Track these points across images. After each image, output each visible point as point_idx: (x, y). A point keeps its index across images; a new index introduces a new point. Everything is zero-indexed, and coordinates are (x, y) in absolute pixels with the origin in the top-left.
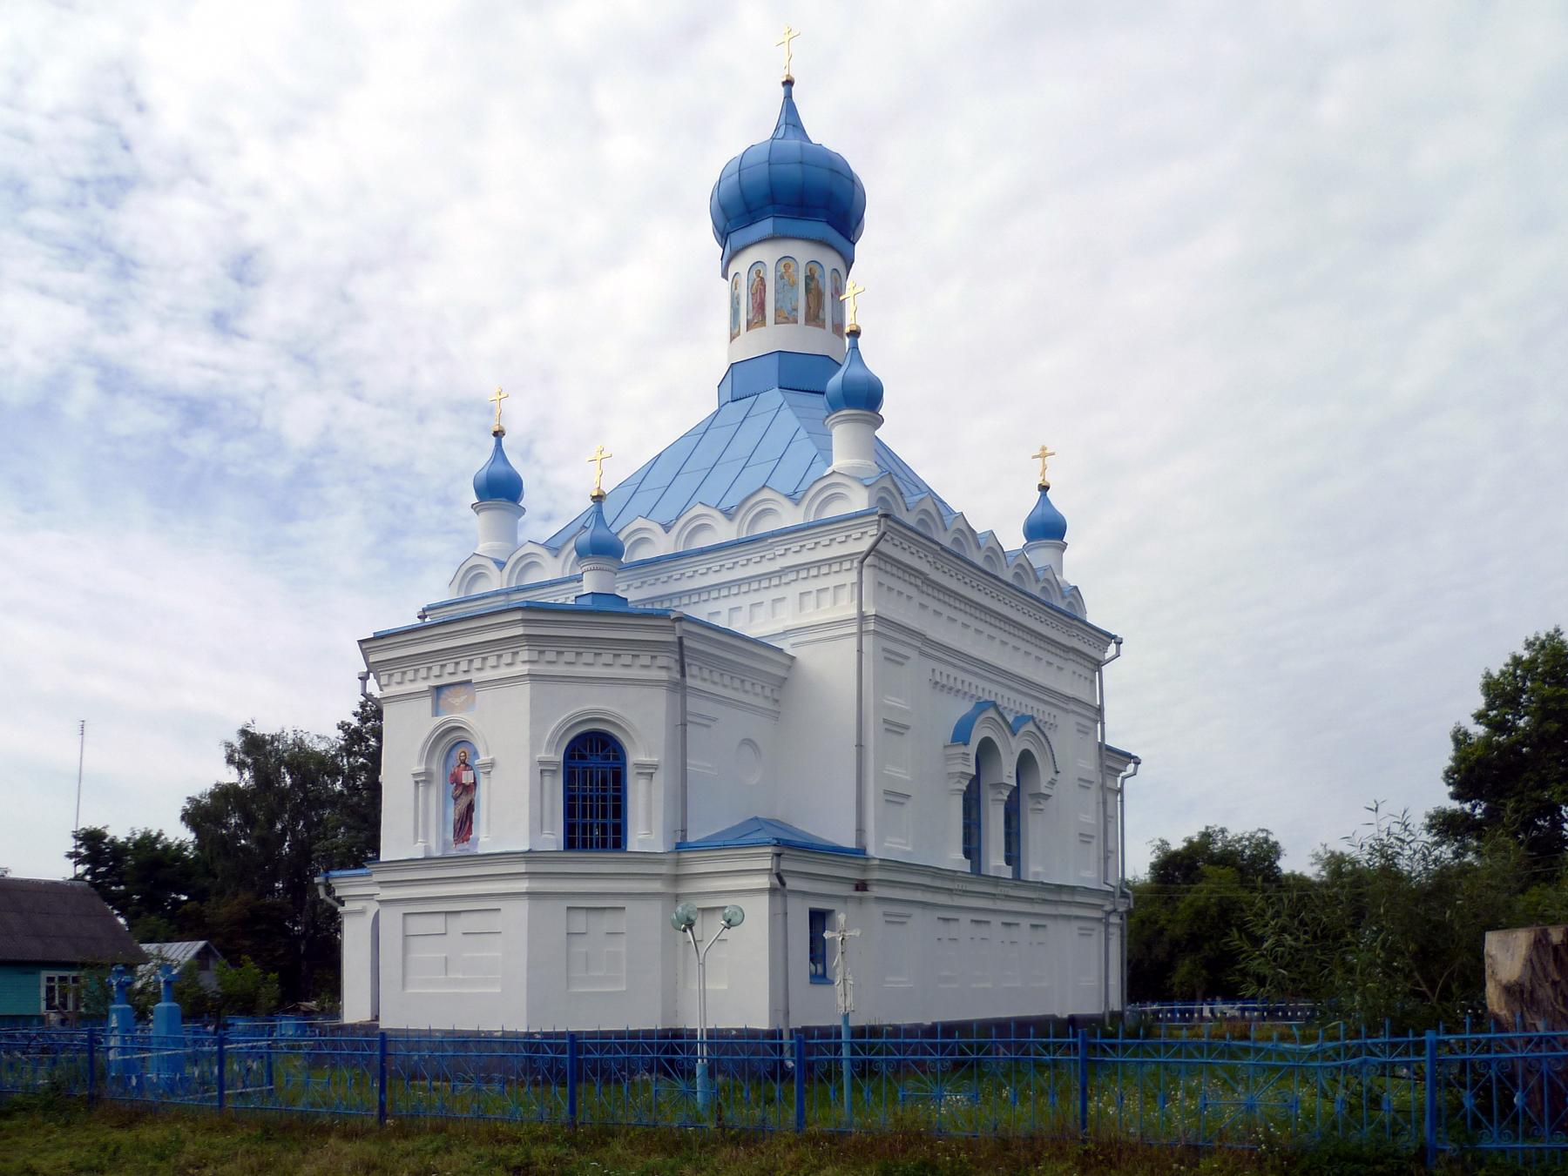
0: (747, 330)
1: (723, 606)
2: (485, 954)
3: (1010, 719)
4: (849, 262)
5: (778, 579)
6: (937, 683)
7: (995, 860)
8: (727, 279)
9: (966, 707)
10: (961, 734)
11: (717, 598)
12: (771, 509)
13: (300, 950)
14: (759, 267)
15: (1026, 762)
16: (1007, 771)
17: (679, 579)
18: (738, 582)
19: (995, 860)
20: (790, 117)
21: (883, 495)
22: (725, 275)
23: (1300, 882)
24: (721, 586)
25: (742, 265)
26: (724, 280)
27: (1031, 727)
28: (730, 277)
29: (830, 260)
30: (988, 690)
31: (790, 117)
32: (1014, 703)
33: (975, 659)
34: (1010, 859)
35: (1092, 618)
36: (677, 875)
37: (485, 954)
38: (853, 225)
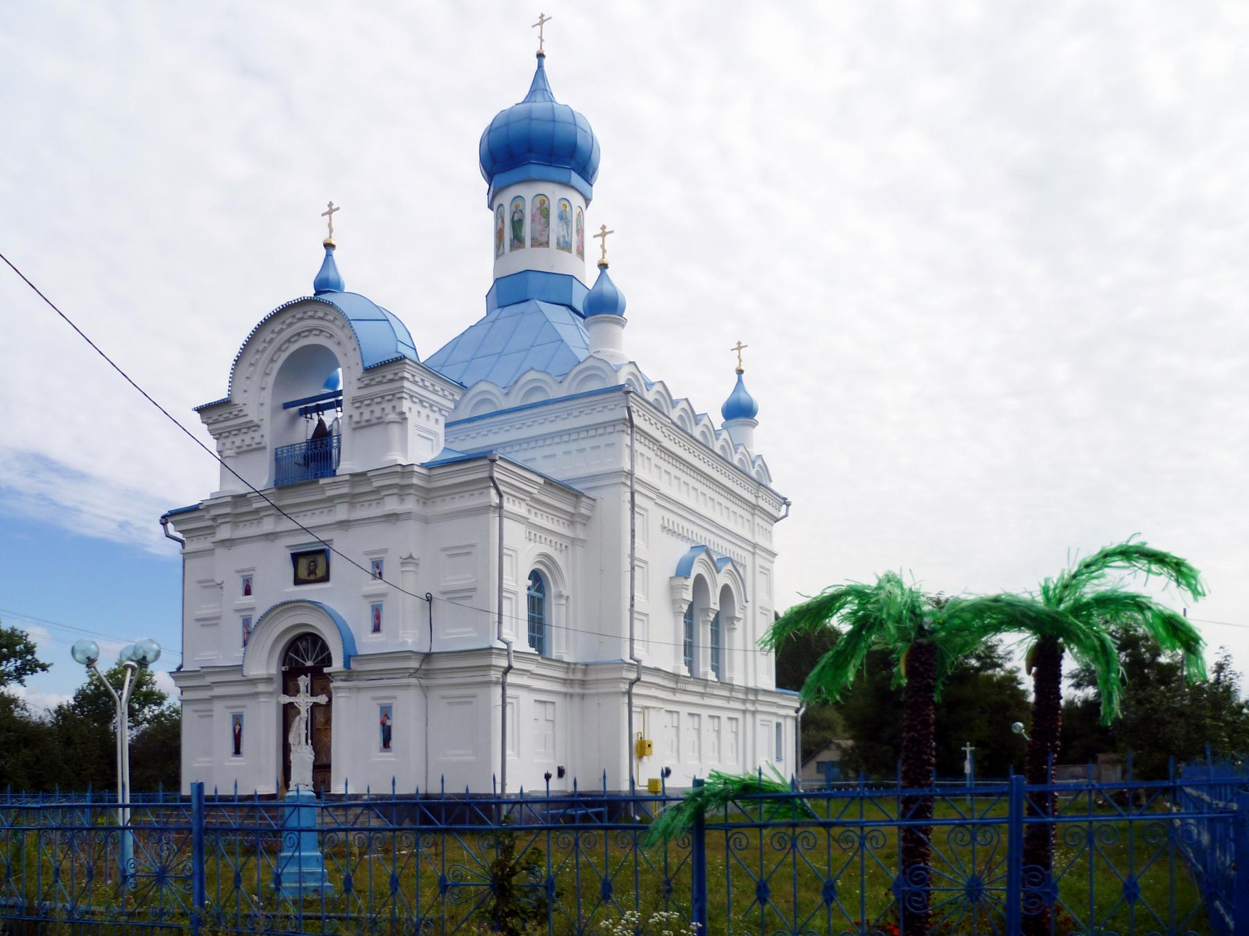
0: (200, 410)
1: (538, 453)
2: (907, 823)
3: (715, 558)
4: (587, 201)
5: (577, 435)
6: (665, 528)
7: (705, 668)
8: (492, 209)
9: (683, 549)
10: (683, 570)
11: (577, 440)
12: (542, 388)
13: (1226, 924)
14: (518, 201)
15: (726, 592)
16: (714, 602)
17: (464, 440)
18: (535, 439)
19: (705, 668)
20: (539, 83)
21: (630, 377)
22: (490, 207)
23: (299, 676)
24: (513, 443)
25: (506, 198)
26: (489, 210)
27: (729, 566)
28: (495, 207)
29: (576, 200)
30: (703, 536)
31: (539, 83)
32: (721, 546)
33: (776, 494)
34: (716, 668)
35: (772, 486)
36: (583, 681)
37: (907, 823)
38: (591, 173)
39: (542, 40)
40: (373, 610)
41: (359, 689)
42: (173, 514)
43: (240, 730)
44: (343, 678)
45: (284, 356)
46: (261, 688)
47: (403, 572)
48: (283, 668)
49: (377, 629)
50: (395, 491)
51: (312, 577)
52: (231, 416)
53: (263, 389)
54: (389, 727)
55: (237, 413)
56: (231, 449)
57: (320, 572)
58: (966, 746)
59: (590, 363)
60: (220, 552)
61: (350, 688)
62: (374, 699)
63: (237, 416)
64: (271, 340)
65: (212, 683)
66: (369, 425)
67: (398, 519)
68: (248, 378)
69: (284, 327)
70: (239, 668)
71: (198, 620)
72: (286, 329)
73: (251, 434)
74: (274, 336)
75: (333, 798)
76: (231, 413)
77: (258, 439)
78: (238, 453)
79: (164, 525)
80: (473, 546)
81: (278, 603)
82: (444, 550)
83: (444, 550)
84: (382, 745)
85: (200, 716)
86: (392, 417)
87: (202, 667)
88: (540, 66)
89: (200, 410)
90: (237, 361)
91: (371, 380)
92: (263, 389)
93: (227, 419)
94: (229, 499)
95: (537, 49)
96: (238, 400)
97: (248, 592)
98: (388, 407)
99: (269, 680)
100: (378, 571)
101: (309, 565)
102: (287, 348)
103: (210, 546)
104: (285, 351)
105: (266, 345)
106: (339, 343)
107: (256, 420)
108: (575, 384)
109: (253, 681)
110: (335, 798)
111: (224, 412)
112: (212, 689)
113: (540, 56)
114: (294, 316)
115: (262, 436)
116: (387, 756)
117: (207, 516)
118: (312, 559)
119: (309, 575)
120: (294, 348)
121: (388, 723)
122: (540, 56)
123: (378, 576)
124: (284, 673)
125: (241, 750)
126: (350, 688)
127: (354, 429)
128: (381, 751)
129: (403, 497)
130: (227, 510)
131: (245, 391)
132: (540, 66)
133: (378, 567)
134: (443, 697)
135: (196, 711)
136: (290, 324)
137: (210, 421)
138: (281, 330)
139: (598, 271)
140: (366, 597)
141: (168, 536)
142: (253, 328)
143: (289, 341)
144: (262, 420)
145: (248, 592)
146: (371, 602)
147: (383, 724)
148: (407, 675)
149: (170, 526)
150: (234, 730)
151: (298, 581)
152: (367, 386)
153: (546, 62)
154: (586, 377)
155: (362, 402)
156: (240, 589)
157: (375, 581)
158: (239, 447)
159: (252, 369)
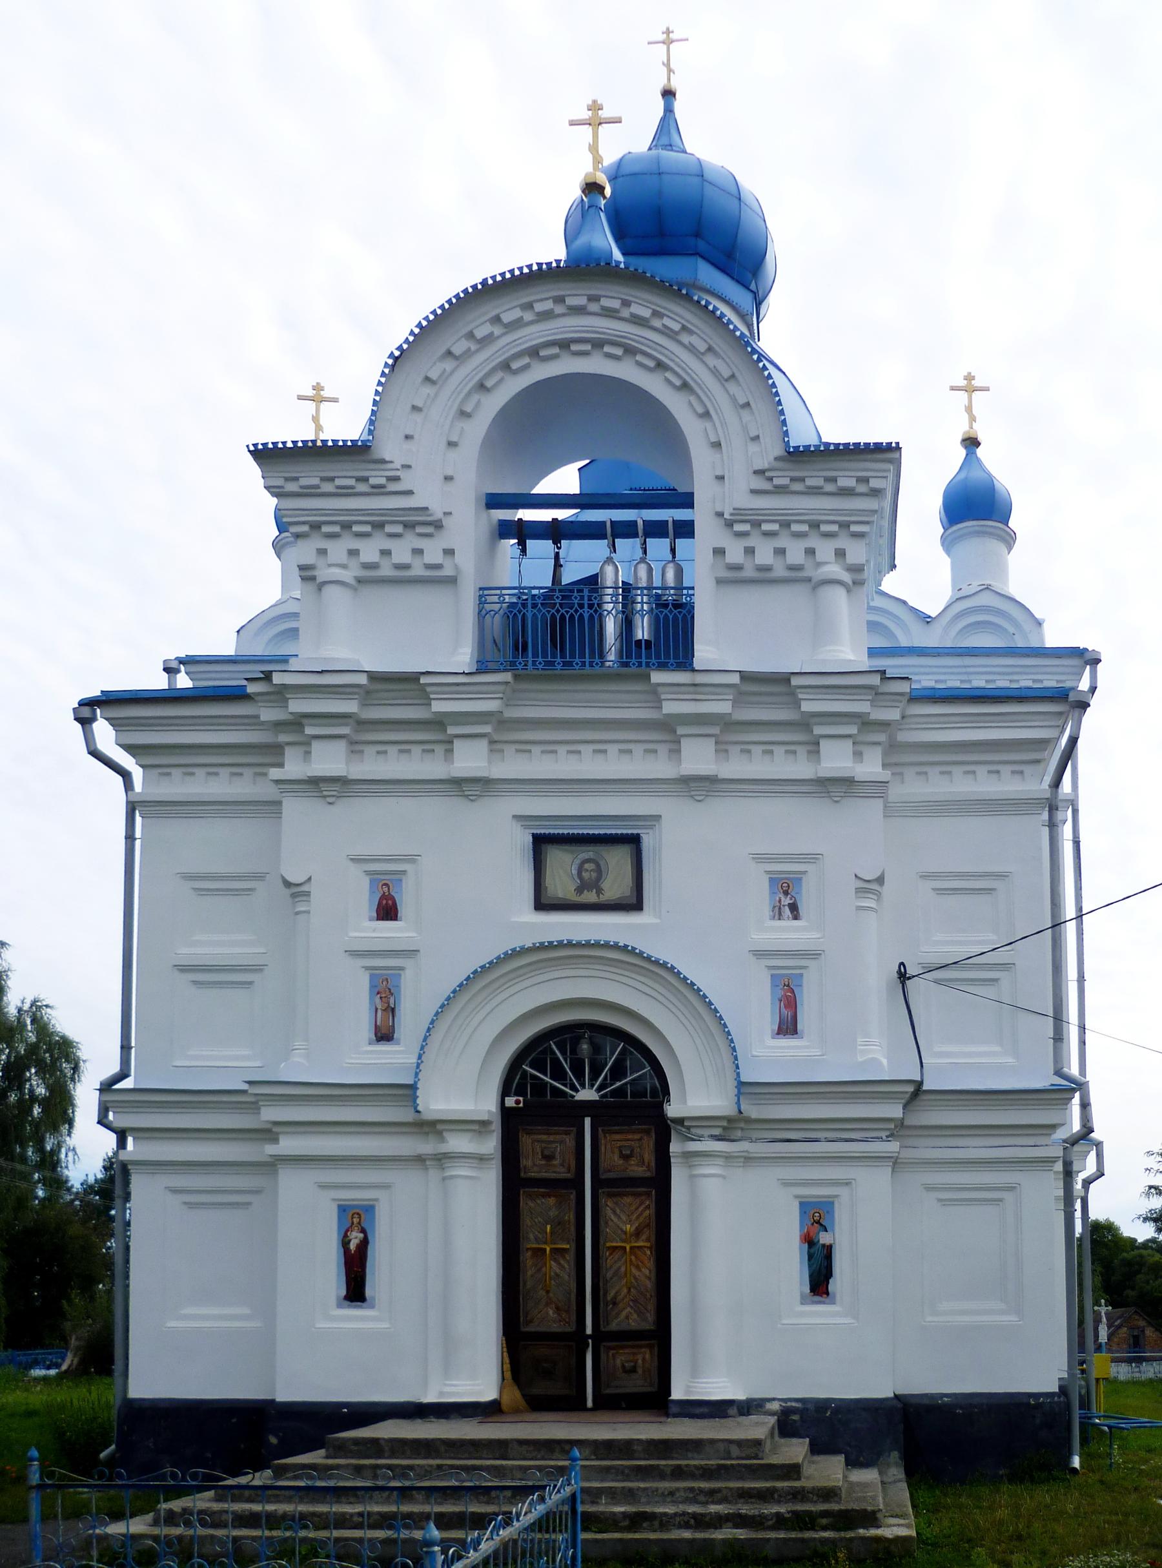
0: (264, 455)
12: (886, 627)
39: (667, 65)
40: (774, 985)
41: (748, 1160)
42: (108, 701)
43: (364, 1244)
44: (717, 1132)
45: (515, 385)
46: (459, 1143)
47: (859, 908)
48: (510, 1102)
49: (788, 1027)
50: (853, 730)
51: (590, 897)
52: (362, 487)
53: (452, 444)
54: (828, 1251)
55: (383, 481)
56: (344, 566)
57: (616, 885)
58: (1100, 1305)
59: (985, 599)
60: (295, 809)
61: (728, 1157)
62: (787, 1184)
63: (379, 490)
64: (489, 339)
65: (277, 1123)
66: (764, 578)
67: (847, 795)
68: (415, 408)
69: (528, 316)
70: (408, 1092)
71: (184, 969)
72: (531, 323)
73: (411, 541)
74: (497, 330)
75: (698, 1411)
76: (365, 479)
77: (433, 554)
78: (360, 581)
79: (85, 722)
80: (1002, 876)
81: (529, 944)
82: (925, 876)
83: (925, 876)
84: (807, 1289)
85: (190, 1205)
86: (834, 570)
87: (250, 1083)
88: (669, 110)
89: (264, 455)
90: (397, 361)
91: (793, 479)
92: (452, 444)
93: (346, 492)
94: (363, 680)
95: (661, 83)
96: (390, 449)
97: (387, 911)
98: (825, 550)
99: (480, 1126)
100: (787, 901)
101: (580, 870)
102: (526, 367)
103: (262, 790)
104: (515, 372)
105: (473, 347)
106: (685, 386)
107: (437, 511)
108: (953, 632)
109: (431, 1127)
110: (705, 1410)
111: (345, 473)
112: (275, 1140)
113: (668, 94)
114: (560, 300)
115: (449, 552)
116: (820, 1313)
117: (268, 714)
118: (591, 855)
119: (580, 890)
120: (596, 365)
121: (824, 1238)
122: (668, 94)
123: (787, 912)
124: (507, 1114)
125: (368, 1292)
126: (728, 1157)
127: (720, 582)
128: (803, 1302)
129: (860, 748)
130: (350, 706)
131: (407, 437)
132: (669, 110)
133: (786, 893)
134: (929, 1188)
135: (175, 1191)
136: (547, 316)
137: (292, 487)
138: (518, 324)
139: (963, 452)
140: (759, 954)
141: (95, 753)
142: (435, 305)
143: (533, 352)
144: (449, 514)
145: (387, 911)
146: (770, 968)
147: (809, 1241)
148: (884, 1134)
149: (103, 731)
150: (345, 1243)
151: (542, 904)
152: (781, 490)
153: (678, 105)
154: (978, 623)
155: (757, 524)
156: (364, 901)
157: (778, 923)
158: (367, 566)
159: (428, 390)
